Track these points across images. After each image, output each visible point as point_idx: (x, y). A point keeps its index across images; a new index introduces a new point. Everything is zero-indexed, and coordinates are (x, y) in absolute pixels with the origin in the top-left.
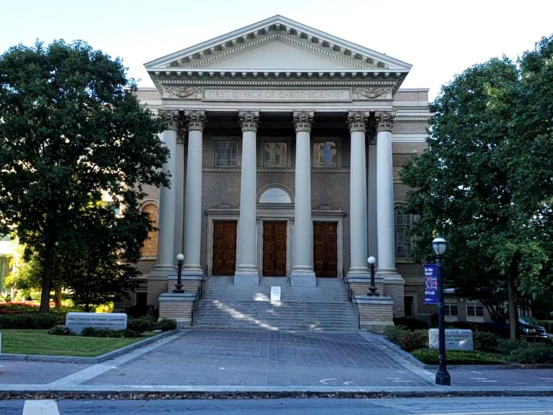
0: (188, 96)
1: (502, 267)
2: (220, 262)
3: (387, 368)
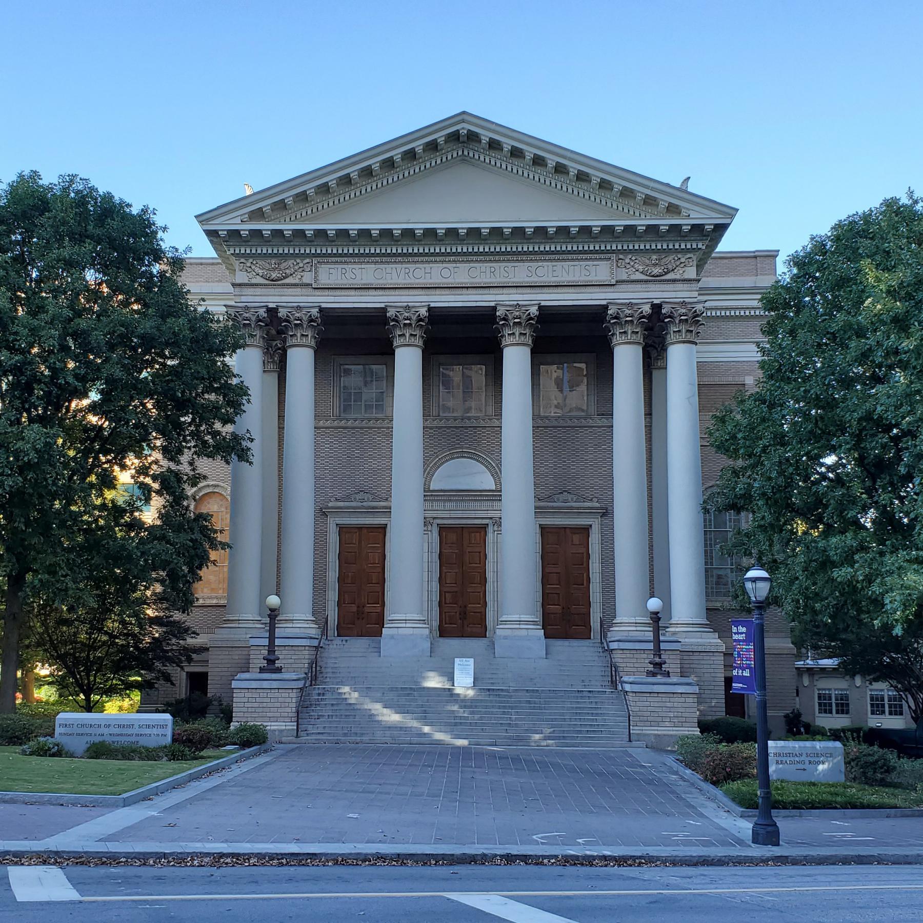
0: (285, 278)
1: (897, 621)
2: (354, 608)
3: (668, 815)
